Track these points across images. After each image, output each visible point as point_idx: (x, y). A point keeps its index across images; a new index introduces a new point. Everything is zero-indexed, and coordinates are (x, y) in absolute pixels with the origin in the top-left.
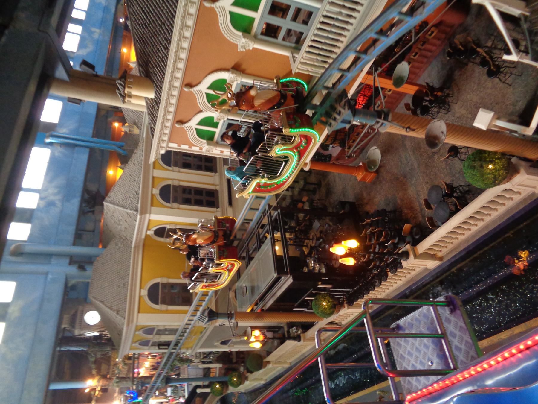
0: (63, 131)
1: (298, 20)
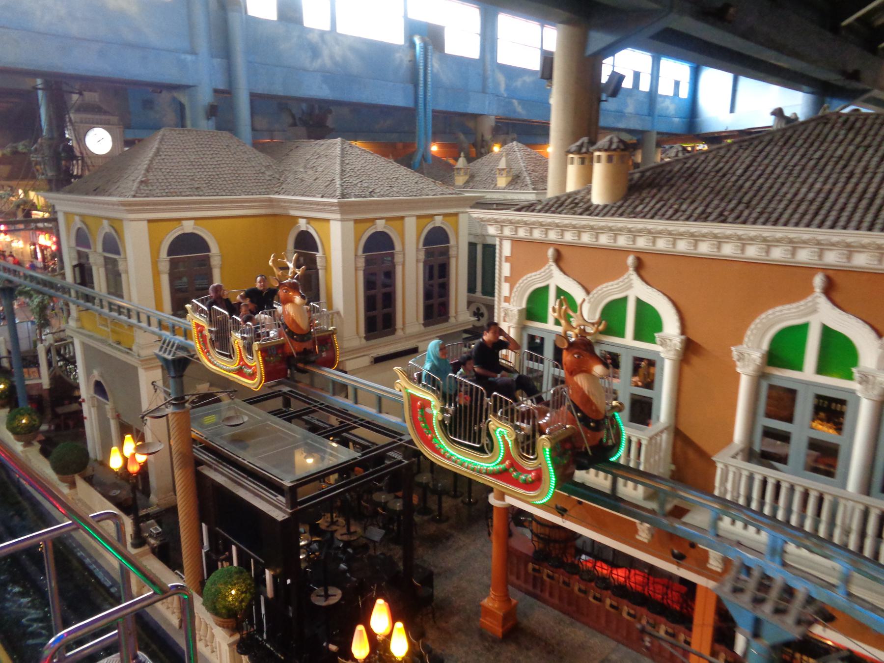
0: (435, 64)
1: (769, 440)
